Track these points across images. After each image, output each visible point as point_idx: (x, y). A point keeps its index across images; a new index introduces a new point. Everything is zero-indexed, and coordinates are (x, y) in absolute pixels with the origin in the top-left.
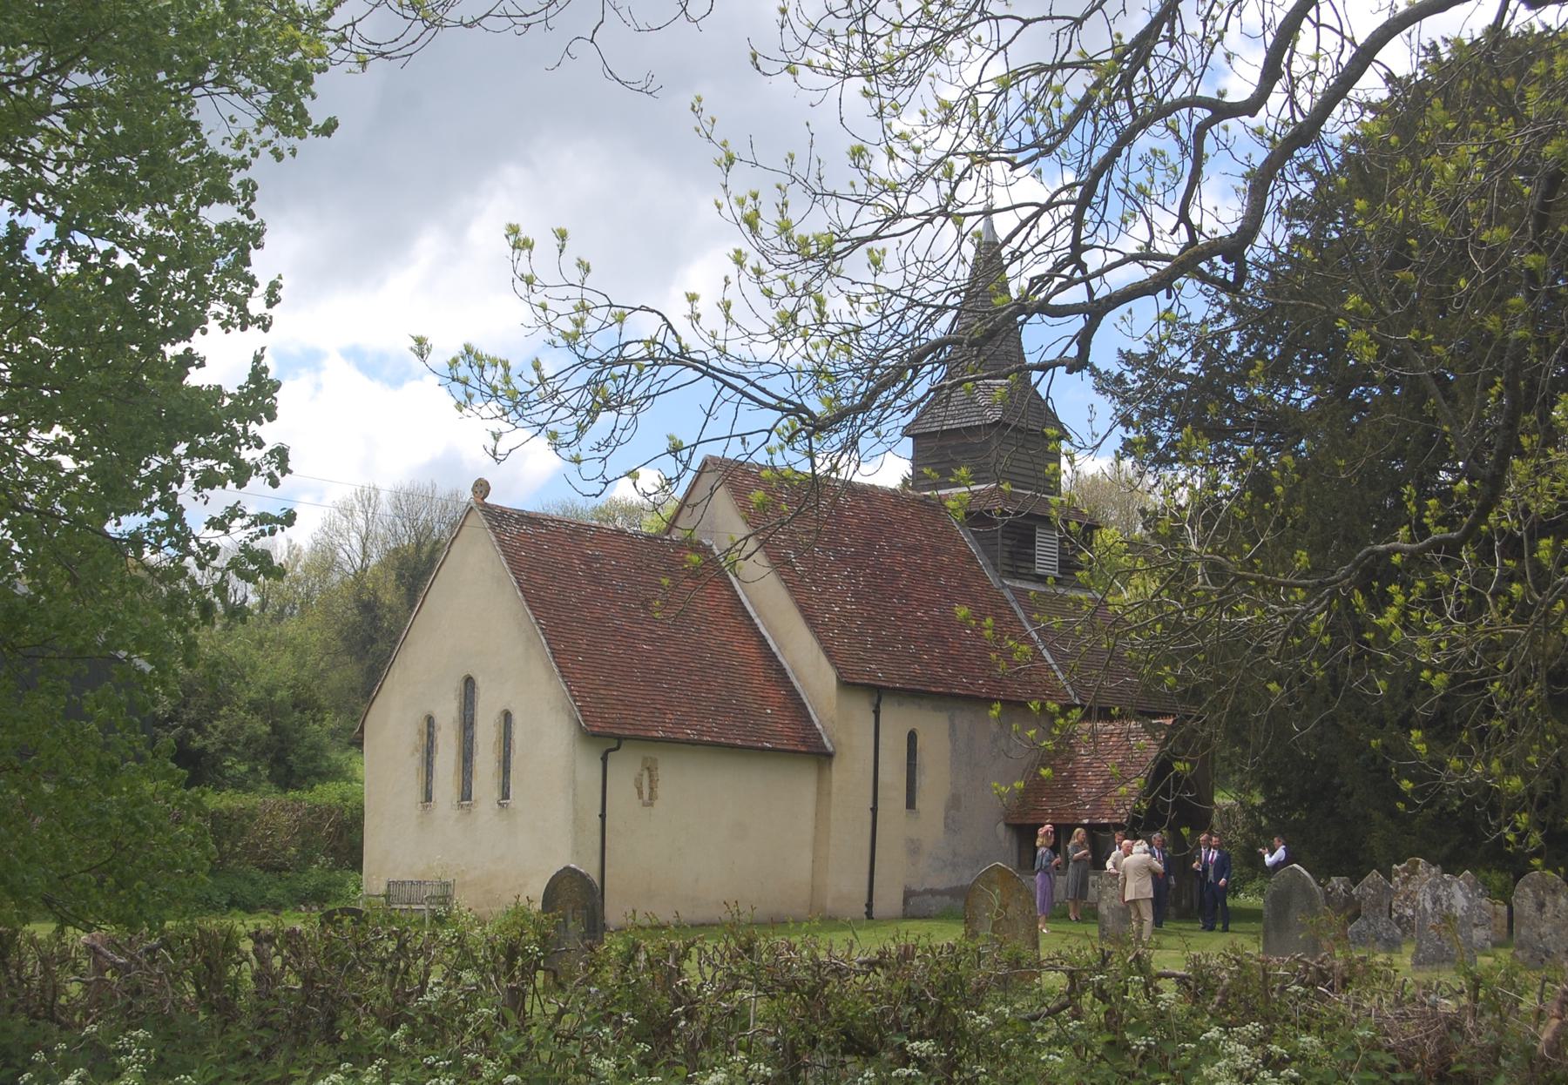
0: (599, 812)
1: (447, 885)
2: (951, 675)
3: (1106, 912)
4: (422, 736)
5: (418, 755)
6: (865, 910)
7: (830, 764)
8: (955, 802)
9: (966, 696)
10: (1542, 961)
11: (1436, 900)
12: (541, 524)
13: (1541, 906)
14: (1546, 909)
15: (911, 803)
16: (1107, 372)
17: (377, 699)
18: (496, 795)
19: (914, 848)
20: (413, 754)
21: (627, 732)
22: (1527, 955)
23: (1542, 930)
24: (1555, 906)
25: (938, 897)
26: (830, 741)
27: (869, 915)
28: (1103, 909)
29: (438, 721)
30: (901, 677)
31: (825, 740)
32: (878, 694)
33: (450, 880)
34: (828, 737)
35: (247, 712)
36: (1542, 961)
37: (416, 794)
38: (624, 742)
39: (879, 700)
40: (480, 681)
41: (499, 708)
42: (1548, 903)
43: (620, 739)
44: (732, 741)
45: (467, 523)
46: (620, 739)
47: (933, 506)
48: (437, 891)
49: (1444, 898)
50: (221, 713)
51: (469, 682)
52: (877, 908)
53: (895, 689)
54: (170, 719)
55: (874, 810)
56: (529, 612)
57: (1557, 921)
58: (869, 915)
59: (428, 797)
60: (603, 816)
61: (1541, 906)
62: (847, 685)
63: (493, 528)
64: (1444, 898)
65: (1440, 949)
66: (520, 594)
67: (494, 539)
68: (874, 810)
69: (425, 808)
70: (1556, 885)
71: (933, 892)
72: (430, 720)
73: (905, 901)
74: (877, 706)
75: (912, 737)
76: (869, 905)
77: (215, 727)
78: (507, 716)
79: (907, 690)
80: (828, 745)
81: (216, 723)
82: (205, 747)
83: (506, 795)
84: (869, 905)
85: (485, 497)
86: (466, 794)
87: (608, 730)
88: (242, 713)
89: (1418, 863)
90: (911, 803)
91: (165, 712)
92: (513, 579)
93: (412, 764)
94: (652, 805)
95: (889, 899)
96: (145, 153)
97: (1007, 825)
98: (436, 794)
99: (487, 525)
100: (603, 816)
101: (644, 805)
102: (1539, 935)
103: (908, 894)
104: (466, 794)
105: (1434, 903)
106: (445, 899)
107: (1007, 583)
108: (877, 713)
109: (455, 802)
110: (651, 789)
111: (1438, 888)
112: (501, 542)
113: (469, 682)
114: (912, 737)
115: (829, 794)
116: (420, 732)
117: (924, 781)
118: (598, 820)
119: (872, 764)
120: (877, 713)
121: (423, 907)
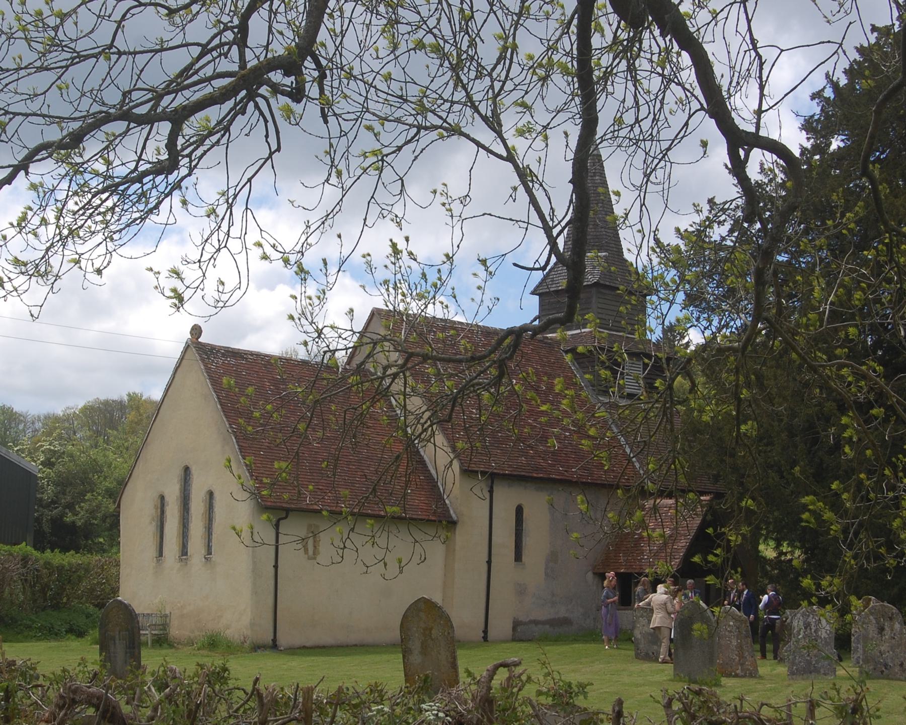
0: (273, 563)
1: (166, 616)
2: (550, 465)
3: (639, 636)
4: (157, 509)
5: (154, 523)
6: (482, 635)
7: (455, 529)
8: (553, 557)
9: (561, 480)
10: (882, 672)
11: (807, 625)
12: (243, 358)
13: (881, 630)
14: (885, 632)
15: (518, 557)
16: (668, 245)
17: (129, 484)
18: (203, 551)
19: (521, 591)
20: (151, 523)
21: (293, 506)
22: (871, 667)
23: (882, 648)
24: (892, 630)
25: (540, 626)
26: (455, 512)
27: (485, 638)
28: (637, 634)
29: (167, 499)
30: (510, 466)
31: (452, 512)
32: (493, 478)
33: (168, 612)
34: (453, 509)
35: (104, 497)
36: (882, 672)
37: (152, 552)
38: (290, 513)
39: (492, 483)
40: (194, 470)
41: (206, 489)
42: (886, 627)
43: (288, 511)
44: (377, 513)
45: (185, 357)
46: (288, 511)
47: (550, 344)
48: (159, 621)
49: (813, 624)
50: (86, 498)
51: (187, 470)
52: (491, 634)
53: (504, 475)
54: (53, 502)
55: (489, 562)
56: (225, 419)
57: (893, 641)
58: (485, 638)
59: (161, 553)
60: (276, 567)
61: (881, 630)
62: (467, 472)
63: (203, 360)
64: (813, 624)
65: (809, 663)
66: (219, 406)
67: (202, 367)
68: (489, 562)
69: (158, 561)
70: (893, 614)
71: (536, 622)
72: (162, 498)
73: (514, 629)
74: (492, 488)
75: (519, 510)
76: (485, 632)
77: (81, 508)
78: (211, 494)
79: (515, 476)
80: (454, 516)
81: (82, 504)
82: (74, 522)
83: (209, 553)
84: (485, 632)
85: (199, 337)
86: (184, 551)
87: (278, 504)
88: (100, 498)
89: (870, 600)
90: (518, 557)
91: (49, 498)
92: (215, 396)
93: (151, 529)
94: (315, 558)
95: (501, 626)
96: (746, 225)
97: (595, 574)
98: (191, 549)
99: (198, 358)
100: (276, 567)
101: (309, 558)
102: (880, 652)
103: (516, 624)
104: (184, 551)
105: (806, 628)
106: (165, 626)
107: (601, 398)
108: (491, 492)
109: (177, 557)
110: (315, 547)
111: (809, 616)
112: (208, 370)
113: (187, 470)
114: (519, 510)
115: (454, 550)
116: (156, 507)
117: (528, 541)
118: (272, 570)
119: (488, 528)
120: (491, 492)
121: (147, 632)
